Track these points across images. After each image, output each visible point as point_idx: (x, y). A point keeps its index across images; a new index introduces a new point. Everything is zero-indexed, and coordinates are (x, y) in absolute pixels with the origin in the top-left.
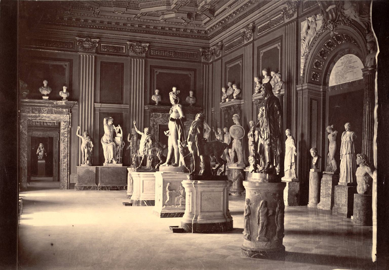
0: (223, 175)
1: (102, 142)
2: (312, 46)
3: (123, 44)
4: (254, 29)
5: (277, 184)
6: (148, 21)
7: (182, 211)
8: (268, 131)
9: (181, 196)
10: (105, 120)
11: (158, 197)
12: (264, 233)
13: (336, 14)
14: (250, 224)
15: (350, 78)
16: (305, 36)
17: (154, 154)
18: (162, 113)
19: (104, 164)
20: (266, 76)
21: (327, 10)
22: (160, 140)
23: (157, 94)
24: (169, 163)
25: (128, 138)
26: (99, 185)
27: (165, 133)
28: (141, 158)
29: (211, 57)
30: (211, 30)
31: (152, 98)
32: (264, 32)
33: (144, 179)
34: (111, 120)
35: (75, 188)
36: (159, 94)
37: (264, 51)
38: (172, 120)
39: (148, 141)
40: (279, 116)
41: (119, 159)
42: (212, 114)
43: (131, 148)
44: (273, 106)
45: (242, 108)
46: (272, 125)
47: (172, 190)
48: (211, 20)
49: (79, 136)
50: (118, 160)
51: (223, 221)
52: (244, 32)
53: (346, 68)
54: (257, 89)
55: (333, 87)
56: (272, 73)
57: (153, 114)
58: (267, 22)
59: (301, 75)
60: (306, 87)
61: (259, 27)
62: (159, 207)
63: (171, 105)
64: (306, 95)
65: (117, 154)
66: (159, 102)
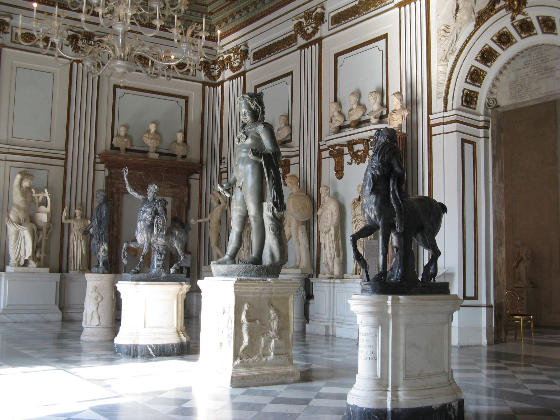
53: (536, 71)
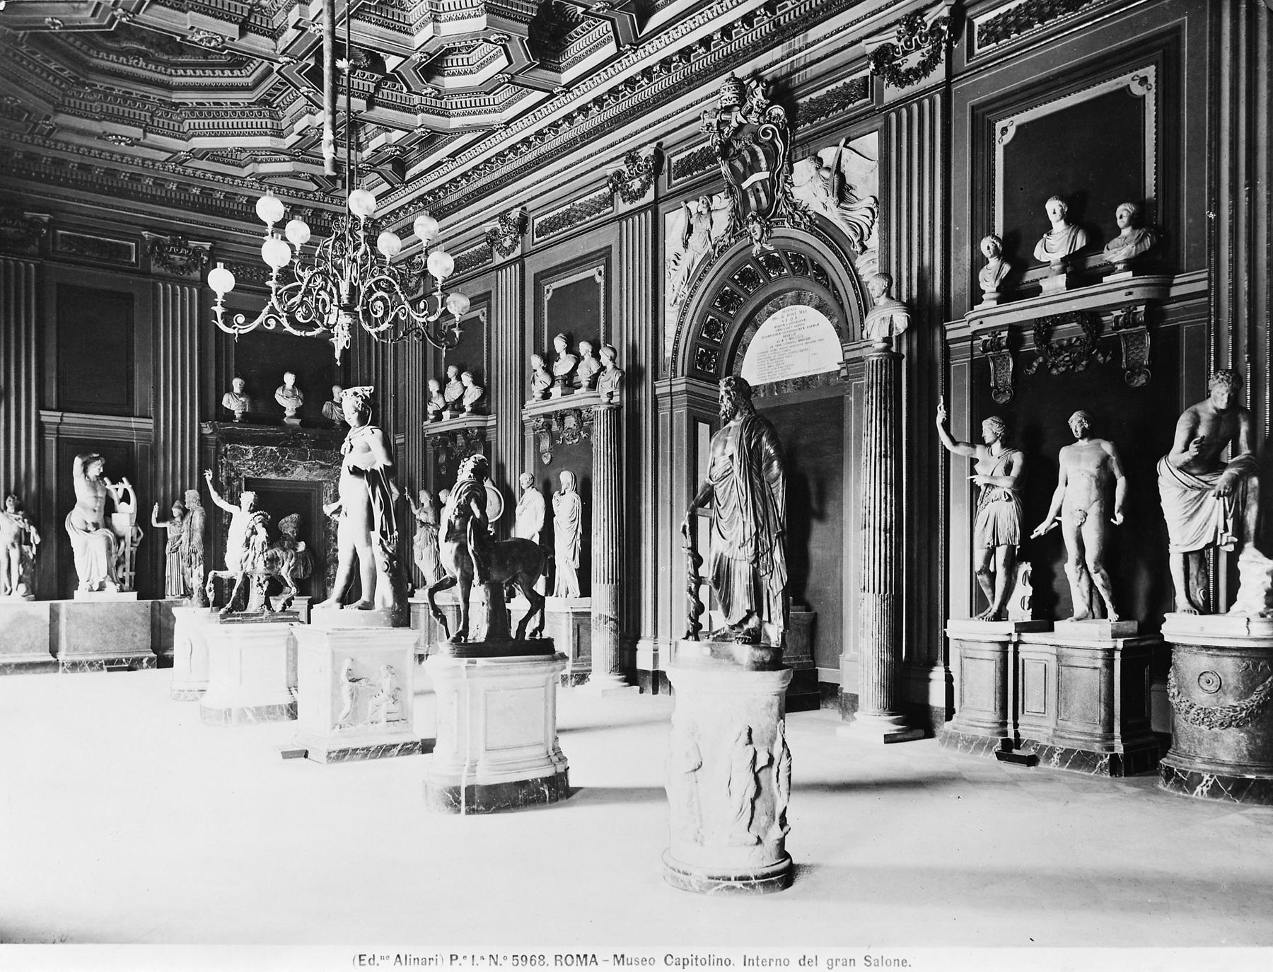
0: (538, 637)
3: (128, 237)
4: (522, 225)
6: (209, 175)
9: (383, 696)
10: (78, 462)
13: (771, 198)
15: (799, 367)
16: (681, 250)
17: (271, 568)
18: (253, 445)
20: (563, 355)
21: (745, 185)
23: (237, 390)
24: (345, 600)
25: (154, 515)
28: (232, 582)
30: (393, 219)
31: (225, 403)
32: (552, 236)
36: (245, 391)
37: (556, 285)
39: (254, 532)
41: (127, 579)
48: (393, 189)
50: (123, 580)
51: (549, 772)
52: (495, 232)
54: (537, 389)
58: (564, 209)
60: (683, 387)
61: (537, 221)
65: (118, 563)
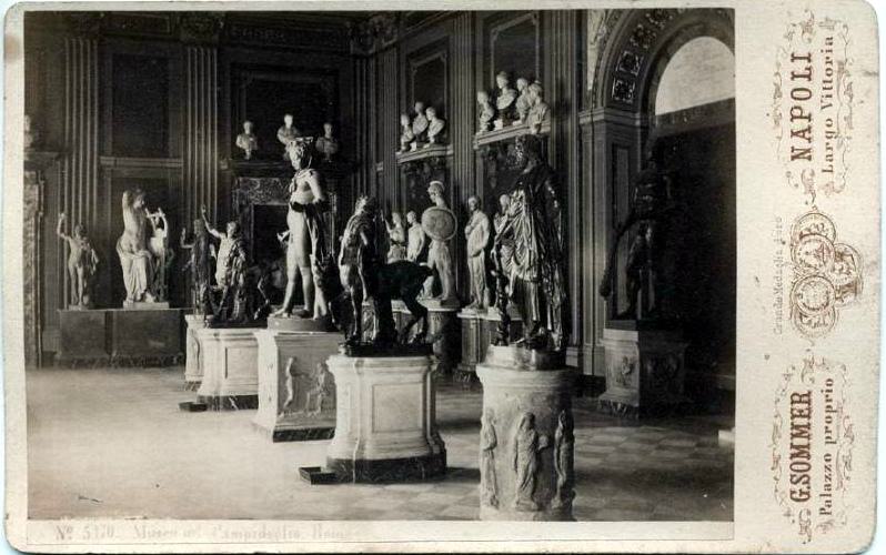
1: (119, 251)
2: (616, 19)
5: (557, 373)
7: (326, 425)
8: (532, 249)
11: (267, 388)
12: (529, 490)
14: (497, 468)
19: (125, 304)
20: (505, 91)
22: (263, 244)
23: (247, 132)
26: (114, 355)
27: (280, 238)
29: (373, 40)
33: (229, 344)
34: (139, 197)
35: (56, 364)
36: (254, 131)
38: (297, 207)
40: (558, 214)
42: (377, 176)
43: (193, 270)
44: (543, 190)
45: (450, 164)
46: (541, 235)
47: (301, 382)
49: (63, 235)
54: (484, 121)
55: (667, 118)
56: (521, 83)
57: (241, 179)
59: (590, 88)
62: (267, 415)
63: (292, 172)
64: (601, 138)
65: (155, 278)
66: (253, 152)
